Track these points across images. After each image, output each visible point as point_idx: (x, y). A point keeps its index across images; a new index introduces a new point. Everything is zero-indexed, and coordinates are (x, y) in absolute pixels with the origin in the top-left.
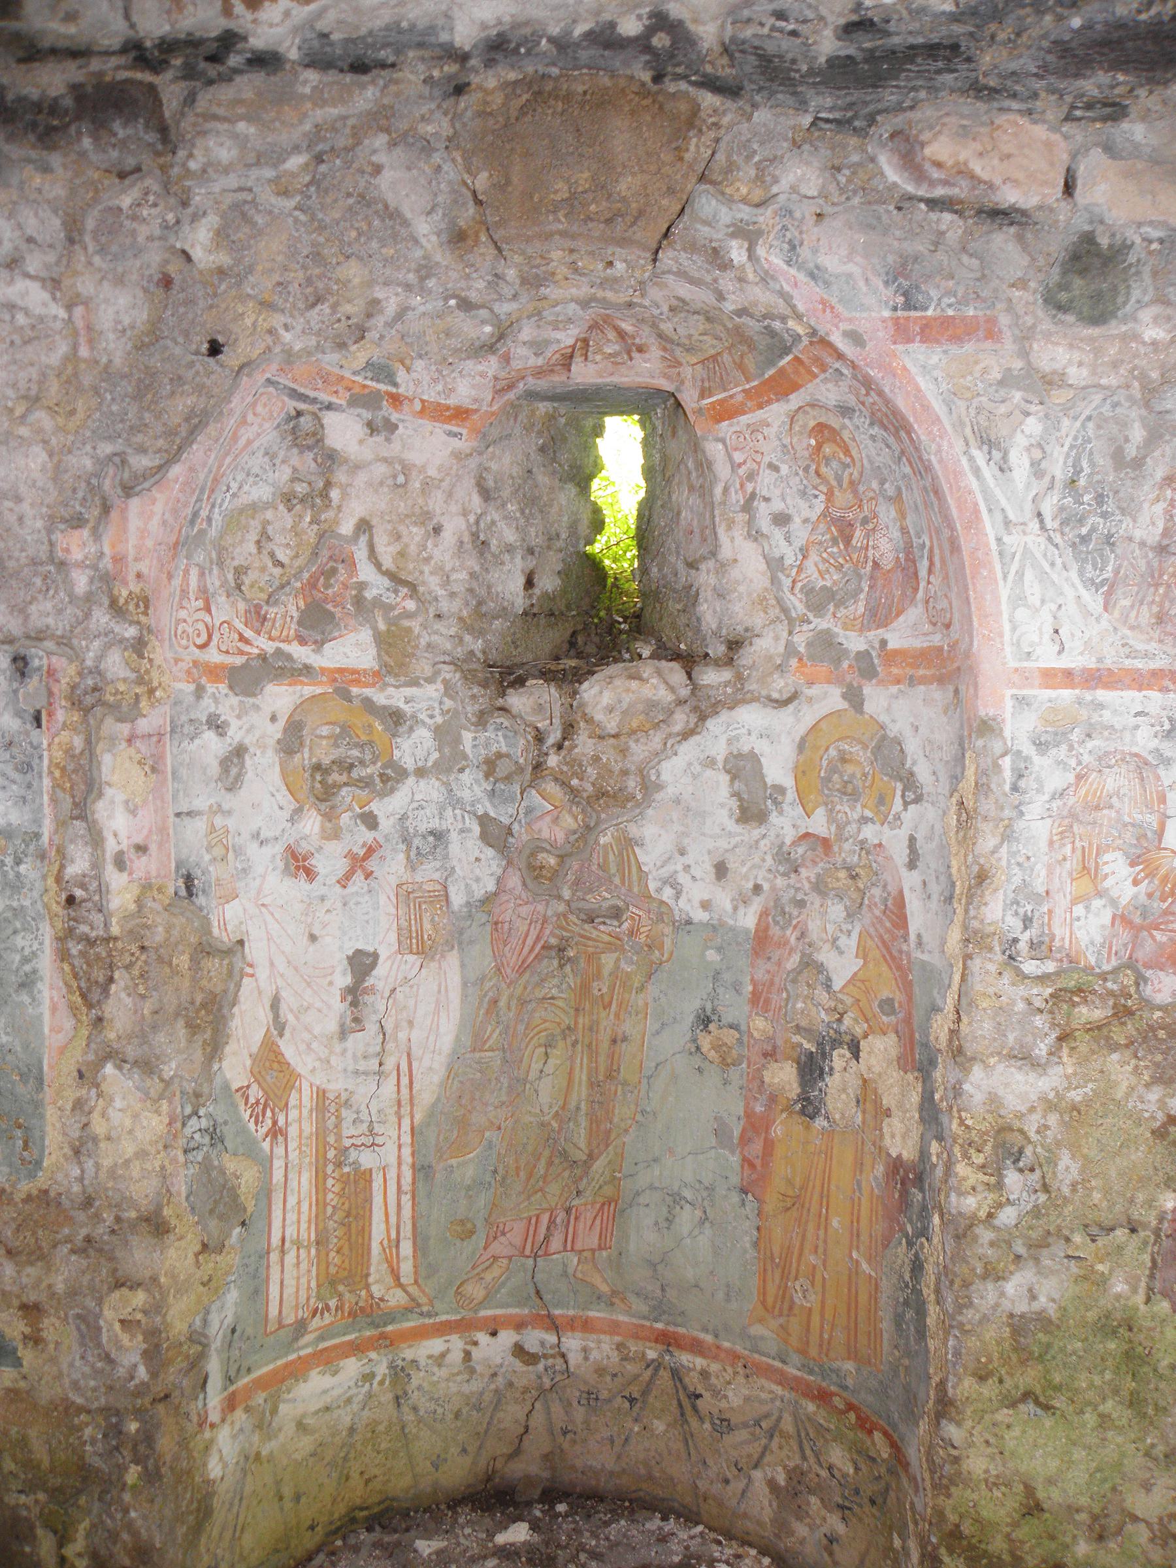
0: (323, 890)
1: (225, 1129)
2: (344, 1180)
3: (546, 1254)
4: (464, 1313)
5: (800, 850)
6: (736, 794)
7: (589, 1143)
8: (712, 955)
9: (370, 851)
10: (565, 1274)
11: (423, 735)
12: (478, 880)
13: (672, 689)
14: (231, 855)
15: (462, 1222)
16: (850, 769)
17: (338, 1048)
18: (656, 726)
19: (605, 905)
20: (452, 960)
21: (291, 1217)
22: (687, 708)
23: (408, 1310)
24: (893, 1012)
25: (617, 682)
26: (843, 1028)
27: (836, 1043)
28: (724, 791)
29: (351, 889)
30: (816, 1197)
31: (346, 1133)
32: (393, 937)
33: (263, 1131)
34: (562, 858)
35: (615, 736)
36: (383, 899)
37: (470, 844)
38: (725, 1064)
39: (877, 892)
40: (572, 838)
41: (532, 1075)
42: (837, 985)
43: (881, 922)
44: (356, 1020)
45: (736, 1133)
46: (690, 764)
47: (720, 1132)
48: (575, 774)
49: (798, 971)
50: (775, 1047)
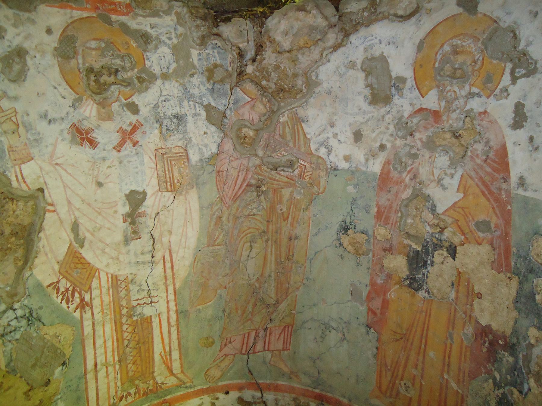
0: (104, 154)
1: (41, 312)
2: (135, 325)
3: (254, 352)
4: (210, 384)
5: (415, 121)
6: (369, 86)
7: (277, 295)
8: (351, 189)
9: (135, 128)
10: (264, 362)
11: (164, 50)
12: (206, 146)
13: (326, 18)
14: (21, 130)
15: (207, 338)
16: (460, 59)
17: (124, 250)
18: (316, 43)
19: (284, 159)
20: (193, 195)
21: (100, 351)
22: (336, 29)
23: (178, 386)
24: (489, 229)
25: (291, 14)
26: (443, 238)
27: (437, 247)
28: (361, 84)
29: (124, 153)
30: (418, 337)
31: (133, 298)
32: (155, 181)
33: (72, 307)
34: (257, 131)
35: (289, 51)
36: (146, 159)
37: (200, 123)
38: (358, 253)
39: (479, 147)
40: (263, 119)
41: (243, 258)
42: (440, 209)
43: (481, 167)
44: (135, 232)
45: (365, 294)
46: (338, 67)
47: (354, 292)
48: (264, 78)
49: (410, 200)
50: (391, 246)
